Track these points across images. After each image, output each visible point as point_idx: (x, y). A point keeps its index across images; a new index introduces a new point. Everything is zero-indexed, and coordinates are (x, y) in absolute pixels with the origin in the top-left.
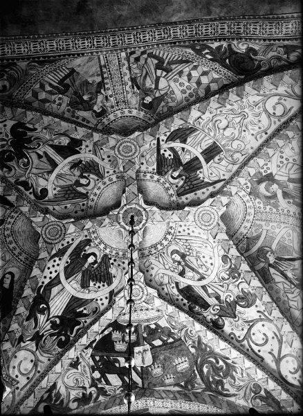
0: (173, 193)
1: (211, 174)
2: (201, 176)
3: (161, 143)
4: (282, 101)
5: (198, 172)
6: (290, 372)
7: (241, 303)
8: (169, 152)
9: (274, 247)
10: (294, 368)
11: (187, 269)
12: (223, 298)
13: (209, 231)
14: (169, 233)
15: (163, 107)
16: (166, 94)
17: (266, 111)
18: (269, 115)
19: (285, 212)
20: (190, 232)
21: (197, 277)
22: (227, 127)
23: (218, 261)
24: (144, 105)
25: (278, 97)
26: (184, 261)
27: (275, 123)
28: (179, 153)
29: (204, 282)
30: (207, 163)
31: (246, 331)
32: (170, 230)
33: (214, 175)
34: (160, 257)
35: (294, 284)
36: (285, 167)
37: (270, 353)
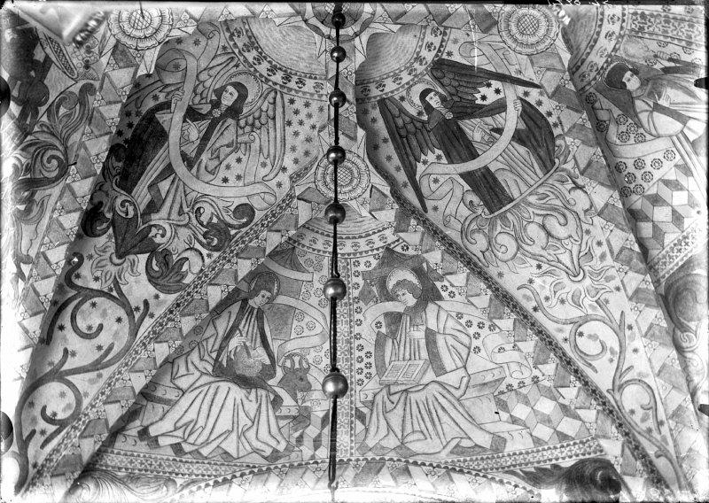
0: (387, 89)
1: (436, 181)
2: (431, 157)
3: (521, 89)
4: (608, 355)
5: (439, 152)
6: (44, 409)
7: (154, 262)
8: (492, 98)
9: (281, 300)
10: (55, 414)
11: (205, 124)
12: (155, 219)
13: (313, 185)
14: (287, 78)
15: (609, 111)
16: (639, 124)
17: (586, 319)
18: (577, 324)
19: (357, 316)
20: (295, 126)
21: (191, 150)
22: (549, 234)
23: (234, 195)
24: (620, 70)
25: (617, 349)
26: (224, 116)
27: (560, 330)
28: (489, 120)
29: (180, 169)
30: (462, 175)
31: (95, 286)
32: (295, 79)
33: (434, 186)
34: (225, 58)
35: (218, 356)
36: (460, 328)
37: (66, 351)
